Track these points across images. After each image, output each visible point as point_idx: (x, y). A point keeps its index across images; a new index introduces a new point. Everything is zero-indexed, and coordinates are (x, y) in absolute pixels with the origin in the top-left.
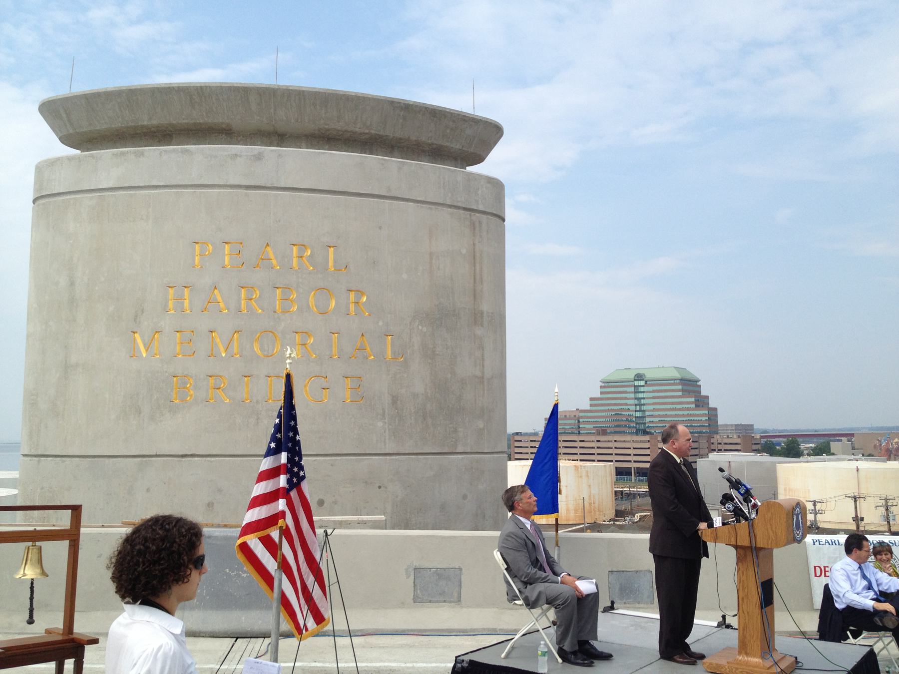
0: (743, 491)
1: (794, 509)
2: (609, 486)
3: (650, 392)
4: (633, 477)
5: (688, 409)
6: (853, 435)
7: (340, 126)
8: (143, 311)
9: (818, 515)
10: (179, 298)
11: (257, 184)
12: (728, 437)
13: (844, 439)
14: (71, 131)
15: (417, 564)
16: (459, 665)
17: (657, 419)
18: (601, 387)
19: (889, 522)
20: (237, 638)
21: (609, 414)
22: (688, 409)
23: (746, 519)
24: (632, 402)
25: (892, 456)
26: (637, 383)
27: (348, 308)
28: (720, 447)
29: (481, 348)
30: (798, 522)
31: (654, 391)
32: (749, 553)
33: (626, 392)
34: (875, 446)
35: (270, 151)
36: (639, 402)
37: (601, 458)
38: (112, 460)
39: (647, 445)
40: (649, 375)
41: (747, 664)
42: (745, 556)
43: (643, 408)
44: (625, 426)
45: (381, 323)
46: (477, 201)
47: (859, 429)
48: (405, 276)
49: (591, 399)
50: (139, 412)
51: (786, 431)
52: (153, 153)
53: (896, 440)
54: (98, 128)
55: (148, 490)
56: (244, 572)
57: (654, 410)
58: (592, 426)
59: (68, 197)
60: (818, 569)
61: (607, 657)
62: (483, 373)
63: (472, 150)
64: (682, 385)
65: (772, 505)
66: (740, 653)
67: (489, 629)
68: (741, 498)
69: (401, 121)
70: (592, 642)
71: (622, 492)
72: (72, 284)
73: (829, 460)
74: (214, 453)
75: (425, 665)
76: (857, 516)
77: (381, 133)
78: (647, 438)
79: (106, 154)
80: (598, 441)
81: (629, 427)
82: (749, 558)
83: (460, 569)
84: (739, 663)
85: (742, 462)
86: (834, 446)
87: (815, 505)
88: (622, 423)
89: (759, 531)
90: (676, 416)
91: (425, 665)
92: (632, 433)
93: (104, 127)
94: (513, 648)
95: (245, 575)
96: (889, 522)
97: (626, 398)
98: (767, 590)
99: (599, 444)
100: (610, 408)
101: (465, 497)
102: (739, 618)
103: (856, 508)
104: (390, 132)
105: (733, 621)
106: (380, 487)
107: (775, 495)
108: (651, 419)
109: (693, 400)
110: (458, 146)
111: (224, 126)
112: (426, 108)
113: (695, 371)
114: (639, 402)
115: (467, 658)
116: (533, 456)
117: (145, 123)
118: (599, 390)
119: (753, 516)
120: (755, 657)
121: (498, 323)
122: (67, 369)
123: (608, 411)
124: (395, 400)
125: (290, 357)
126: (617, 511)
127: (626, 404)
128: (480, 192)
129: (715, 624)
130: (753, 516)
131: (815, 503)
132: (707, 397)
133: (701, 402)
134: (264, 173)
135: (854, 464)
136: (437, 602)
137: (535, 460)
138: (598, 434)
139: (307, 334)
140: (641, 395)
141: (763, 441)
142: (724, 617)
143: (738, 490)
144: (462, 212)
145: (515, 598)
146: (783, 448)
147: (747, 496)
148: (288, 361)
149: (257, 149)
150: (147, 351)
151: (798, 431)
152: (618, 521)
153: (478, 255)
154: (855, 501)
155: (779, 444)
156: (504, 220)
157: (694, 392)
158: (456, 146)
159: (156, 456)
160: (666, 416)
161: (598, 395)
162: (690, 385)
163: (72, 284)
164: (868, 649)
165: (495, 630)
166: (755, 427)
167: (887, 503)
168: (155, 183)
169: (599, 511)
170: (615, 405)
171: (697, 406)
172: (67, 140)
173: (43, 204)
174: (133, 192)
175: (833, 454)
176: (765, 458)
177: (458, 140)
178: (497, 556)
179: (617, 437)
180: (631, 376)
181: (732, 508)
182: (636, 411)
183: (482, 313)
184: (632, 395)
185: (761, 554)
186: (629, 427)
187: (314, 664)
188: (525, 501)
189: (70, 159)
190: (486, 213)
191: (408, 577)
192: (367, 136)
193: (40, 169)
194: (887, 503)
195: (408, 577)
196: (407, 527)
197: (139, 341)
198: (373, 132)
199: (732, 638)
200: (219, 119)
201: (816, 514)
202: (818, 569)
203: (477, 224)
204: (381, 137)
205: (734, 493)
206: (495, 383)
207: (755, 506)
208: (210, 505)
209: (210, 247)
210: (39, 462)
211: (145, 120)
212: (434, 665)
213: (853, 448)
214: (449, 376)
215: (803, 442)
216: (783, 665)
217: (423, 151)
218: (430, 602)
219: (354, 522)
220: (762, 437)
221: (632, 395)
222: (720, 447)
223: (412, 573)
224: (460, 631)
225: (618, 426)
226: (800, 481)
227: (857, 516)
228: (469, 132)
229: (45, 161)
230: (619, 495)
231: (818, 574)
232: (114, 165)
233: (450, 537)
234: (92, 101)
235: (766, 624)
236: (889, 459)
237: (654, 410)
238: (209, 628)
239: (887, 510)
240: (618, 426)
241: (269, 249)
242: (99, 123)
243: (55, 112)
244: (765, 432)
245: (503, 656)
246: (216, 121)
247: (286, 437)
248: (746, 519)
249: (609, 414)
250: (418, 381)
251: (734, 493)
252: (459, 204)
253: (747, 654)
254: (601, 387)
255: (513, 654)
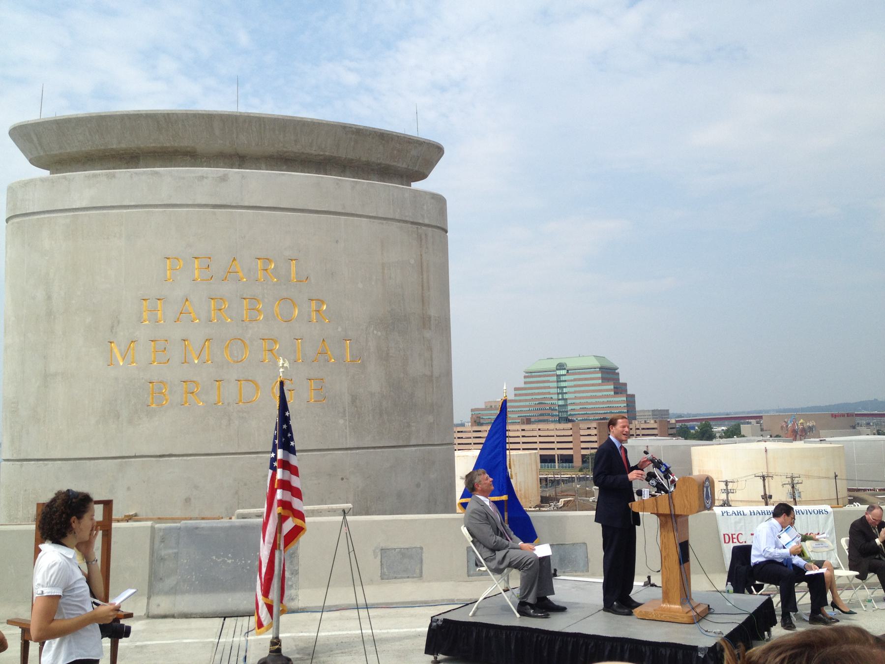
0: (663, 469)
1: (704, 483)
2: (534, 473)
3: (571, 381)
4: (557, 464)
5: (607, 396)
6: (761, 417)
7: (296, 149)
8: (119, 322)
9: (730, 495)
10: (154, 310)
11: (224, 203)
12: (645, 422)
13: (753, 421)
14: (42, 154)
15: (383, 545)
16: (434, 624)
17: (578, 407)
18: (525, 377)
19: (795, 499)
20: (225, 618)
21: (533, 403)
22: (607, 396)
23: (666, 492)
24: (555, 391)
25: (798, 437)
26: (558, 372)
27: (309, 316)
28: (638, 432)
29: (430, 349)
30: (704, 492)
31: (575, 380)
32: (669, 520)
33: (548, 381)
34: (782, 427)
35: (234, 173)
36: (561, 390)
37: (526, 446)
38: (93, 462)
39: (570, 432)
40: (570, 364)
41: (670, 610)
42: (667, 522)
43: (566, 396)
44: (549, 415)
45: (340, 329)
46: (423, 216)
47: (767, 411)
48: (360, 286)
49: (516, 389)
50: (118, 416)
51: (700, 415)
52: (124, 175)
53: (802, 421)
54: (69, 150)
55: (129, 489)
56: (229, 558)
57: (576, 398)
58: (516, 416)
59: (42, 216)
60: (727, 537)
61: (561, 609)
62: (432, 372)
63: (416, 169)
64: (602, 373)
65: (687, 480)
66: (664, 602)
67: (449, 600)
68: (662, 475)
69: (352, 144)
70: (550, 597)
71: (546, 479)
72: (49, 298)
73: (740, 442)
74: (190, 452)
75: (397, 630)
76: (765, 494)
77: (335, 155)
78: (569, 425)
79: (79, 176)
80: (523, 430)
81: (552, 416)
82: (670, 524)
83: (421, 548)
84: (663, 610)
85: (660, 446)
86: (744, 429)
87: (727, 485)
88: (547, 412)
89: (677, 501)
90: (596, 403)
91: (397, 630)
92: (554, 421)
93: (75, 150)
94: (477, 608)
95: (230, 561)
96: (795, 499)
97: (549, 387)
98: (684, 549)
99: (524, 433)
100: (534, 397)
101: (418, 485)
102: (662, 574)
103: (764, 486)
104: (342, 154)
105: (657, 579)
106: (342, 479)
107: (691, 473)
108: (573, 407)
109: (612, 387)
110: (404, 166)
111: (189, 149)
112: (375, 132)
113: (614, 360)
114: (561, 390)
115: (441, 618)
116: (481, 446)
117: (114, 147)
118: (523, 380)
119: (672, 489)
120: (675, 604)
121: (443, 325)
122: (47, 378)
123: (532, 400)
124: (354, 399)
125: (283, 367)
126: (542, 497)
127: (549, 393)
128: (425, 207)
129: (642, 584)
130: (672, 489)
131: (727, 483)
132: (625, 385)
133: (620, 389)
134: (228, 194)
135: (762, 445)
136: (401, 578)
137: (482, 450)
138: (523, 423)
139: (274, 341)
140: (563, 384)
141: (678, 425)
142: (649, 578)
143: (659, 468)
144: (410, 225)
145: (478, 564)
146: (697, 432)
147: (667, 473)
148: (281, 370)
149: (222, 171)
150: (124, 359)
151: (710, 414)
152: (543, 507)
153: (425, 264)
154: (764, 480)
155: (693, 428)
156: (446, 232)
157: (613, 379)
158: (402, 165)
159: (135, 457)
160: (587, 403)
161: (523, 385)
162: (609, 373)
163: (49, 298)
164: (767, 597)
165: (453, 600)
166: (671, 412)
167: (793, 481)
168: (125, 203)
169: (525, 497)
170: (539, 394)
171: (616, 393)
172: (37, 162)
173: (18, 223)
174: (105, 211)
175: (744, 436)
176: (681, 442)
177: (399, 159)
178: (464, 530)
179: (541, 426)
180: (553, 365)
181: (655, 484)
182: (559, 400)
183: (430, 318)
184: (555, 385)
185: (679, 520)
186: (552, 416)
187: (301, 634)
188: (482, 482)
189: (43, 180)
190: (430, 226)
191: (375, 558)
192: (321, 157)
193: (12, 190)
194: (793, 481)
195: (375, 558)
196: (367, 514)
197: (116, 350)
198: (327, 154)
199: (658, 593)
200: (186, 142)
201: (728, 493)
202: (727, 537)
203: (423, 237)
204: (335, 158)
205: (656, 471)
206: (441, 381)
207: (673, 481)
208: (188, 500)
209: (182, 263)
210: (21, 466)
211: (114, 144)
212: (405, 630)
213: (762, 430)
214: (402, 375)
215: (715, 425)
216: (699, 610)
217: (372, 170)
218: (395, 578)
219: (325, 510)
220: (677, 421)
221: (555, 385)
222: (638, 432)
223: (379, 554)
224: (422, 602)
225: (541, 415)
226: (710, 459)
227: (765, 494)
228: (414, 152)
229: (19, 182)
230: (544, 482)
231: (727, 540)
232: (85, 187)
233: (386, 521)
234: (61, 127)
235: (684, 576)
236: (795, 439)
237: (576, 398)
238: (198, 610)
239: (793, 487)
240: (541, 415)
241: (236, 262)
242: (71, 146)
243: (24, 135)
244: (680, 416)
245: (471, 614)
246: (182, 145)
247: (284, 437)
248: (666, 492)
249: (533, 403)
250: (375, 381)
251: (656, 471)
252: (407, 219)
253: (669, 602)
254: (525, 377)
255: (478, 613)
